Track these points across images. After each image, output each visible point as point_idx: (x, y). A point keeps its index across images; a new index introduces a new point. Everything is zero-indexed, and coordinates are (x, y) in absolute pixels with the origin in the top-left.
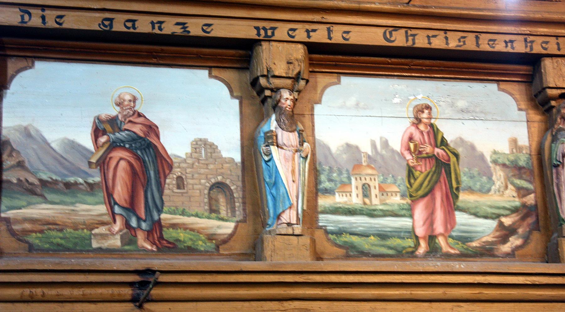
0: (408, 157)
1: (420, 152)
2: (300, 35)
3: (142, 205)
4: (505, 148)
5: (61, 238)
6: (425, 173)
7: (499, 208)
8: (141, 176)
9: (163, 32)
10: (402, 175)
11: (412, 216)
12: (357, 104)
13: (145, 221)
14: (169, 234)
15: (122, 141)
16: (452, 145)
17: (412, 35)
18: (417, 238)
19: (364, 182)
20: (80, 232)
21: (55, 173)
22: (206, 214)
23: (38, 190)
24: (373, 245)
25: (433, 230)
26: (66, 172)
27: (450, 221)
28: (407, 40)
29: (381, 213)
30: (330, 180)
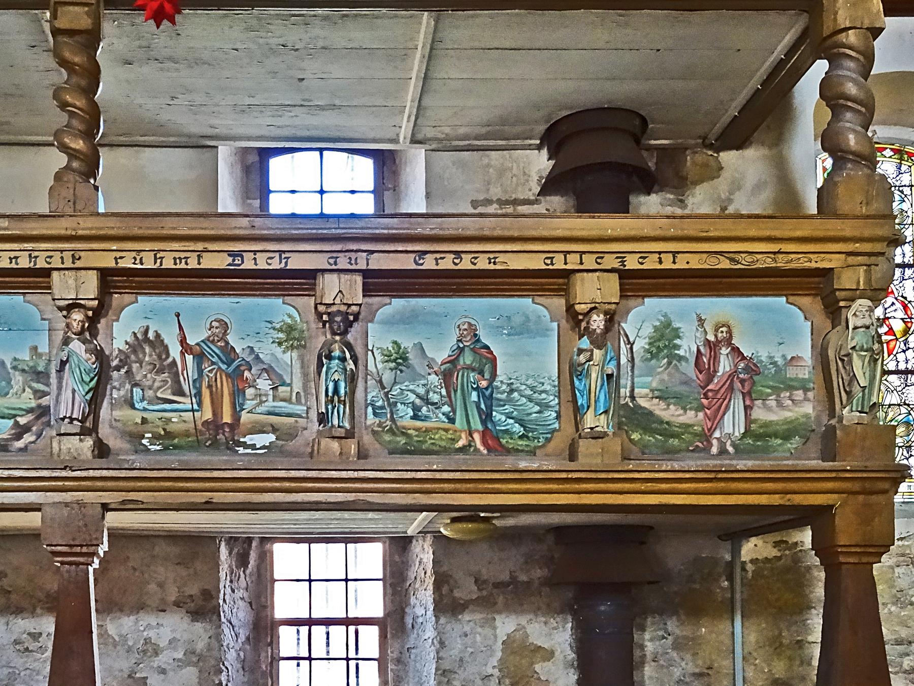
2: (611, 262)
7: (14, 409)
28: (155, 263)
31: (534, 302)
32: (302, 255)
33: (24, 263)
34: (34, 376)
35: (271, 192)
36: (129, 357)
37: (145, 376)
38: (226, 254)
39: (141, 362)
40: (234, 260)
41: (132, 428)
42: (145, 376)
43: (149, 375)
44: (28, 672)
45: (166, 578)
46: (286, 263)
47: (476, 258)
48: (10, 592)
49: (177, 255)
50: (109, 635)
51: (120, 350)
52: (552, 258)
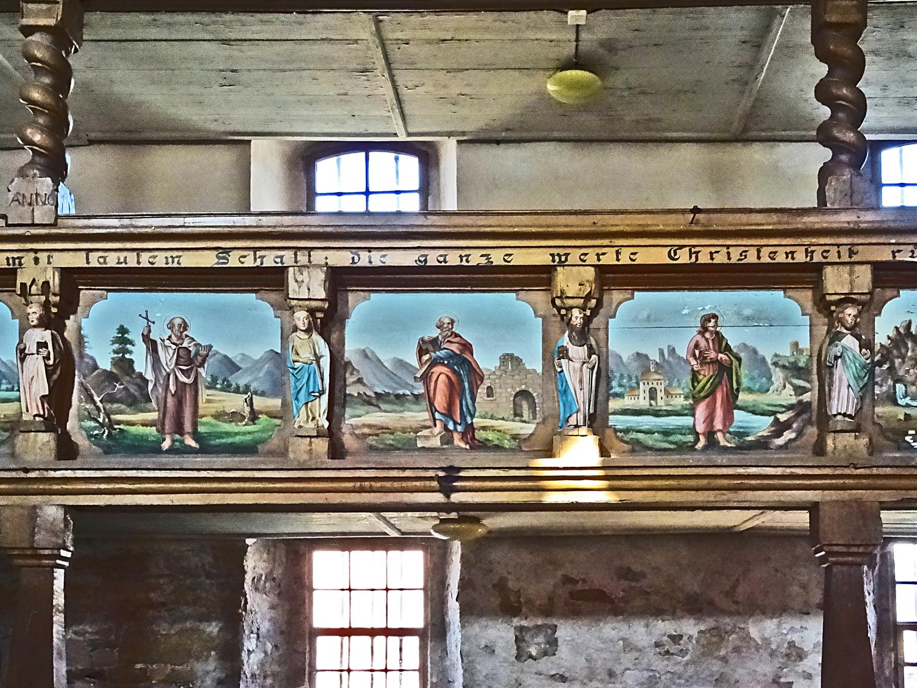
0: (693, 362)
1: (705, 358)
2: (592, 259)
3: (458, 411)
4: (786, 351)
5: (393, 440)
6: (708, 377)
7: (776, 406)
8: (457, 387)
10: (687, 379)
11: (693, 415)
12: (649, 317)
13: (460, 424)
14: (480, 435)
15: (442, 358)
16: (735, 351)
17: (695, 252)
18: (697, 434)
19: (651, 386)
22: (512, 417)
23: (374, 401)
24: (656, 441)
25: (713, 427)
26: (395, 385)
27: (728, 418)
28: (690, 258)
29: (664, 413)
30: (620, 386)
31: (785, 296)
33: (800, 257)
34: (796, 373)
36: (891, 352)
37: (908, 372)
39: (903, 357)
41: (895, 425)
42: (908, 372)
43: (911, 371)
44: (669, 675)
45: (810, 580)
48: (648, 593)
50: (751, 638)
51: (881, 345)
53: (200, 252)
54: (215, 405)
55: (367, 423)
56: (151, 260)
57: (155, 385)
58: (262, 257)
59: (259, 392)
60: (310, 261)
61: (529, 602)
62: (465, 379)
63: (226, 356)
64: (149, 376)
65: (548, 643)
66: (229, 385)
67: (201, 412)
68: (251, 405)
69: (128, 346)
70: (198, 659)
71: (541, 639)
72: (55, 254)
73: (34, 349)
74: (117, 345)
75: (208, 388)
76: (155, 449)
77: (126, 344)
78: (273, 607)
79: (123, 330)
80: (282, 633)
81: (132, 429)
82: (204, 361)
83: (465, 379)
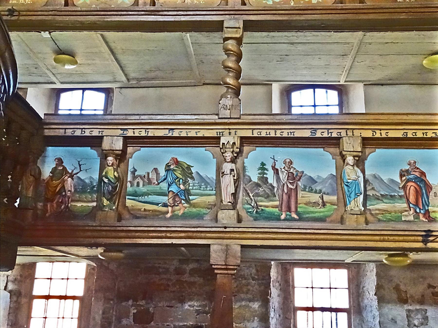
3: (421, 204)
8: (419, 191)
9: (427, 137)
15: (412, 179)
17: (330, 133)
20: (397, 214)
21: (387, 192)
23: (381, 198)
28: (328, 134)
31: (324, 150)
32: (394, 131)
35: (292, 106)
38: (120, 130)
40: (124, 132)
46: (148, 133)
47: (92, 131)
49: (289, 131)
52: (416, 133)
53: (303, 130)
54: (306, 199)
55: (377, 208)
56: (281, 133)
57: (278, 189)
58: (331, 133)
59: (326, 193)
60: (353, 135)
61: (412, 297)
62: (423, 189)
63: (310, 176)
64: (275, 185)
65: (423, 318)
66: (312, 190)
67: (299, 202)
68: (323, 199)
69: (265, 171)
70: (248, 321)
71: (419, 316)
72: (238, 130)
73: (229, 172)
74: (260, 171)
75: (302, 191)
76: (278, 219)
77: (264, 170)
78: (279, 296)
79: (263, 164)
80: (281, 309)
81: (267, 209)
82: (300, 178)
83: (423, 189)
